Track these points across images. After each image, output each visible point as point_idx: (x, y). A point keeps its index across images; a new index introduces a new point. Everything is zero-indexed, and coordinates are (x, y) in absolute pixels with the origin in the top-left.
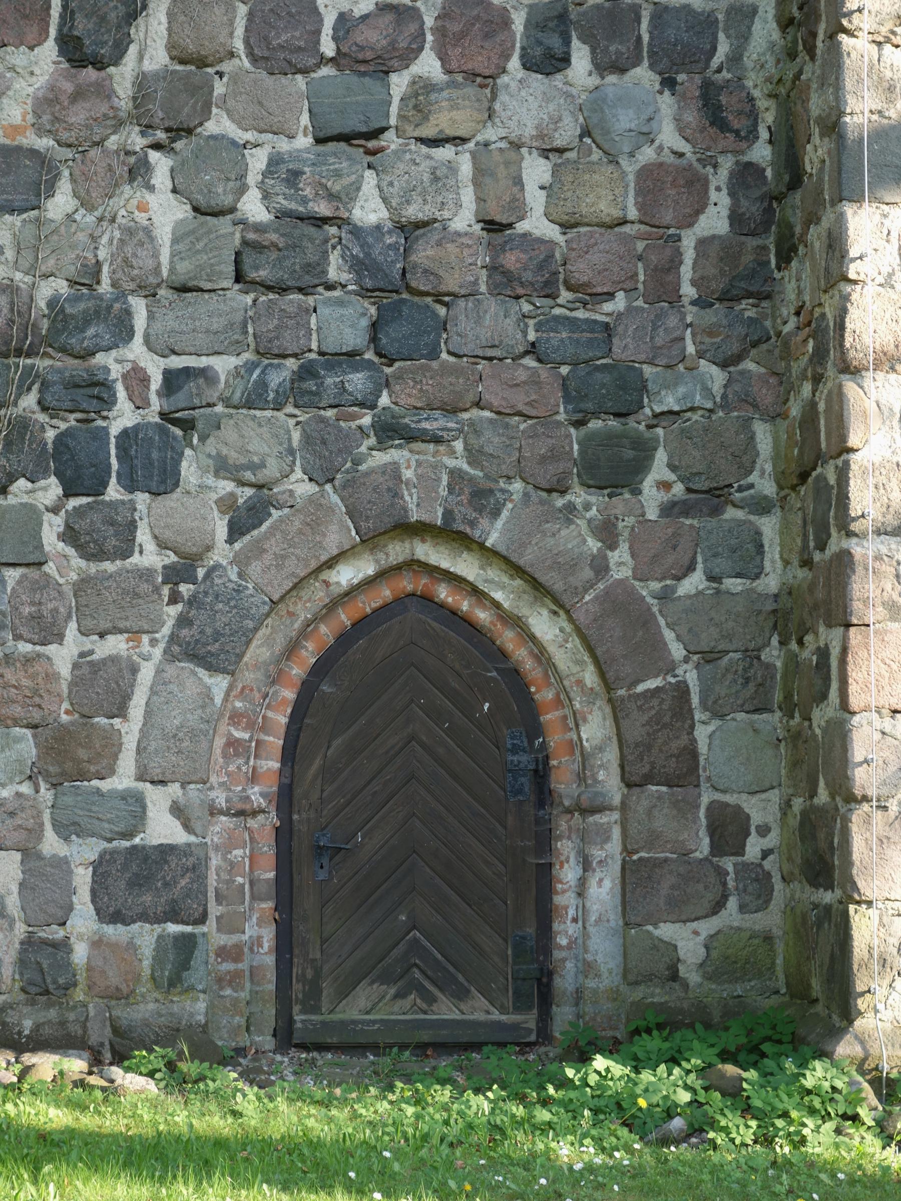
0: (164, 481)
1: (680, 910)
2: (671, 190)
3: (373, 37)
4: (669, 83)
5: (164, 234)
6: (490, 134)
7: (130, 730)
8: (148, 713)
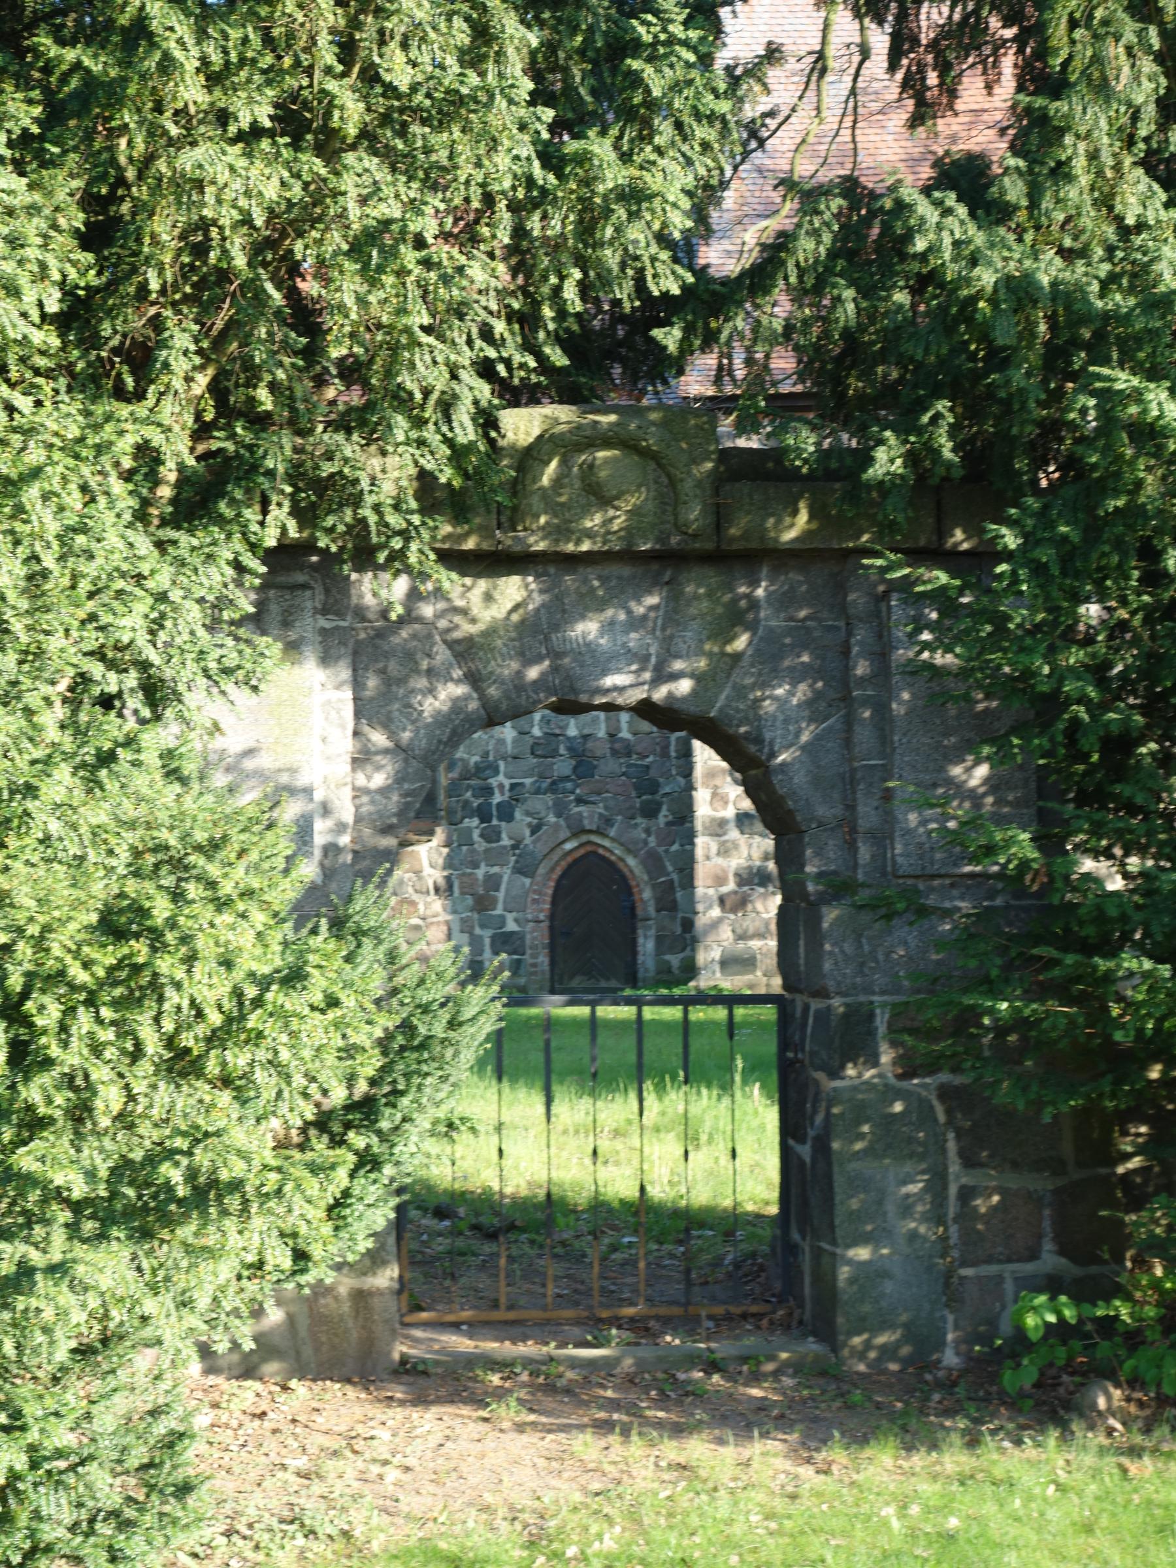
5: (509, 741)
7: (501, 895)
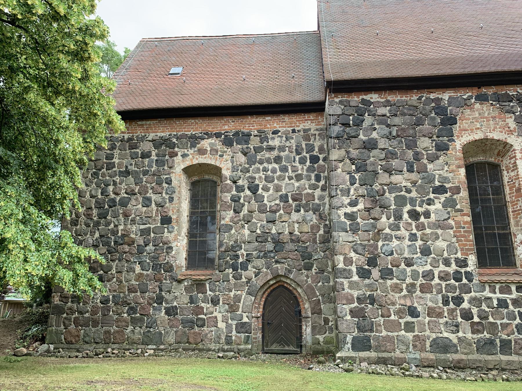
0: (246, 269)
1: (320, 333)
2: (315, 228)
3: (274, 208)
4: (314, 213)
5: (246, 235)
6: (290, 220)
7: (241, 305)
8: (243, 302)
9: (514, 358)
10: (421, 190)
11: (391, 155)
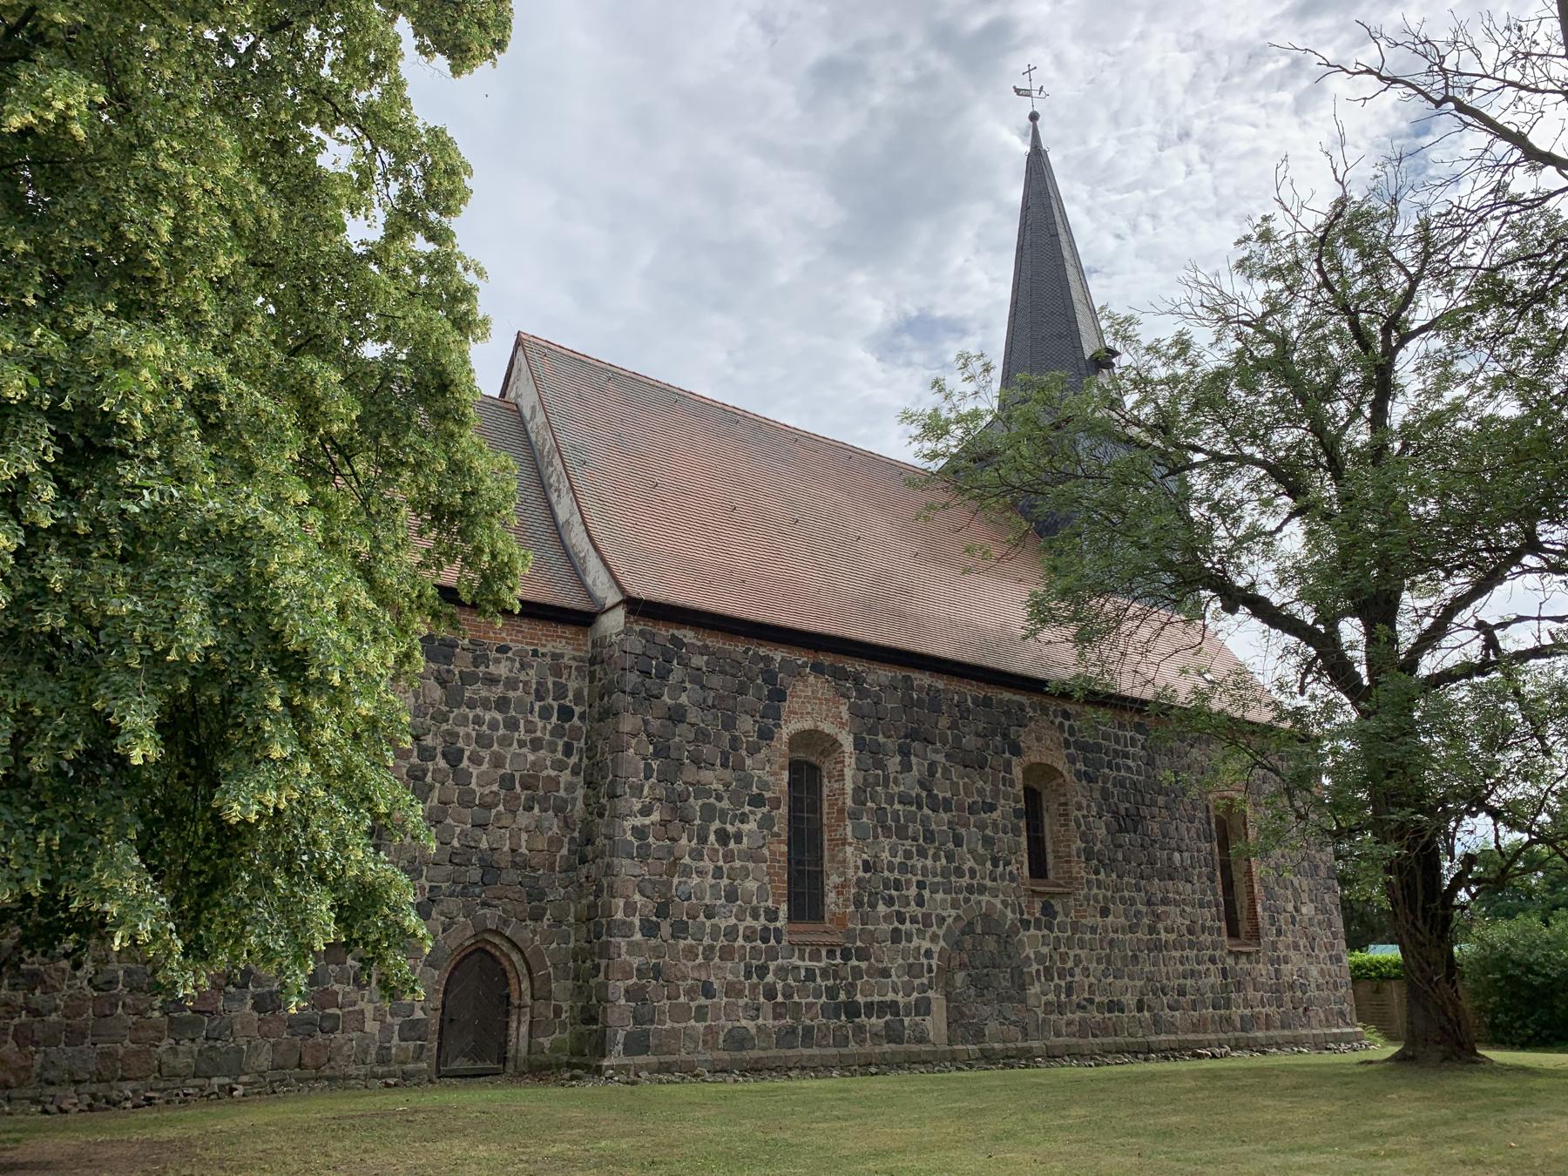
2: (555, 842)
3: (488, 799)
9: (815, 1051)
10: (736, 800)
11: (702, 736)
